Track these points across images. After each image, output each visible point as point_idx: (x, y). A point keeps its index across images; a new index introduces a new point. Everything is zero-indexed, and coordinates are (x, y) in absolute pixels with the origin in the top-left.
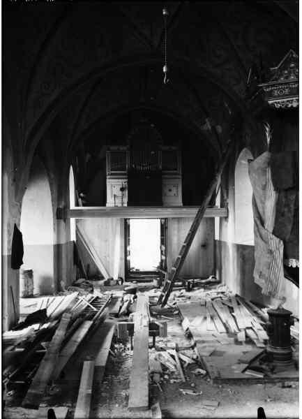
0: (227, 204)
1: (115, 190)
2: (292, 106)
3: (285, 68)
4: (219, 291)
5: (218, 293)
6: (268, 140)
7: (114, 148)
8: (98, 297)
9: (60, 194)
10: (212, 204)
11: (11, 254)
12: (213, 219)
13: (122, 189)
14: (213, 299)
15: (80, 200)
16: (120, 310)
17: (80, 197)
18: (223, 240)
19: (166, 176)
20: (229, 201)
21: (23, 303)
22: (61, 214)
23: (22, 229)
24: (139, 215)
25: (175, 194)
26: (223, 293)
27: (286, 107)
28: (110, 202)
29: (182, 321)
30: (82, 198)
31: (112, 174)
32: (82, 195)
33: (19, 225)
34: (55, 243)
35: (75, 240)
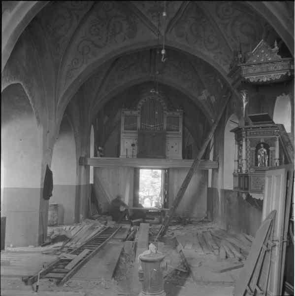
0: (218, 158)
1: (127, 144)
2: (263, 81)
3: (257, 53)
4: (210, 227)
5: (208, 229)
6: (245, 105)
7: (128, 113)
8: (109, 228)
9: (82, 145)
10: (206, 157)
11: (43, 187)
12: (207, 171)
13: (133, 145)
14: (203, 232)
15: (98, 152)
16: (127, 237)
17: (99, 150)
18: (214, 187)
19: (169, 136)
20: (219, 156)
21: (49, 230)
22: (82, 162)
23: (52, 169)
24: (146, 165)
25: (175, 147)
26: (211, 228)
27: (258, 81)
28: (123, 152)
29: (177, 246)
30: (101, 151)
31: (125, 133)
32: (100, 148)
33: (50, 166)
34: (77, 184)
35: (92, 183)
